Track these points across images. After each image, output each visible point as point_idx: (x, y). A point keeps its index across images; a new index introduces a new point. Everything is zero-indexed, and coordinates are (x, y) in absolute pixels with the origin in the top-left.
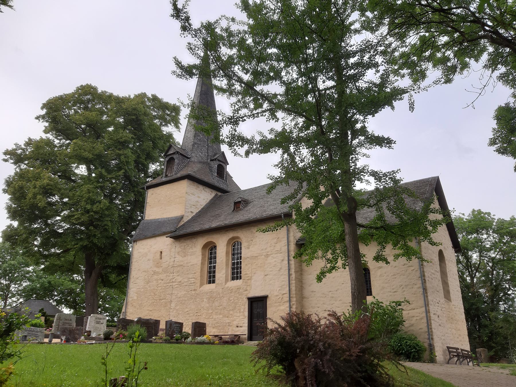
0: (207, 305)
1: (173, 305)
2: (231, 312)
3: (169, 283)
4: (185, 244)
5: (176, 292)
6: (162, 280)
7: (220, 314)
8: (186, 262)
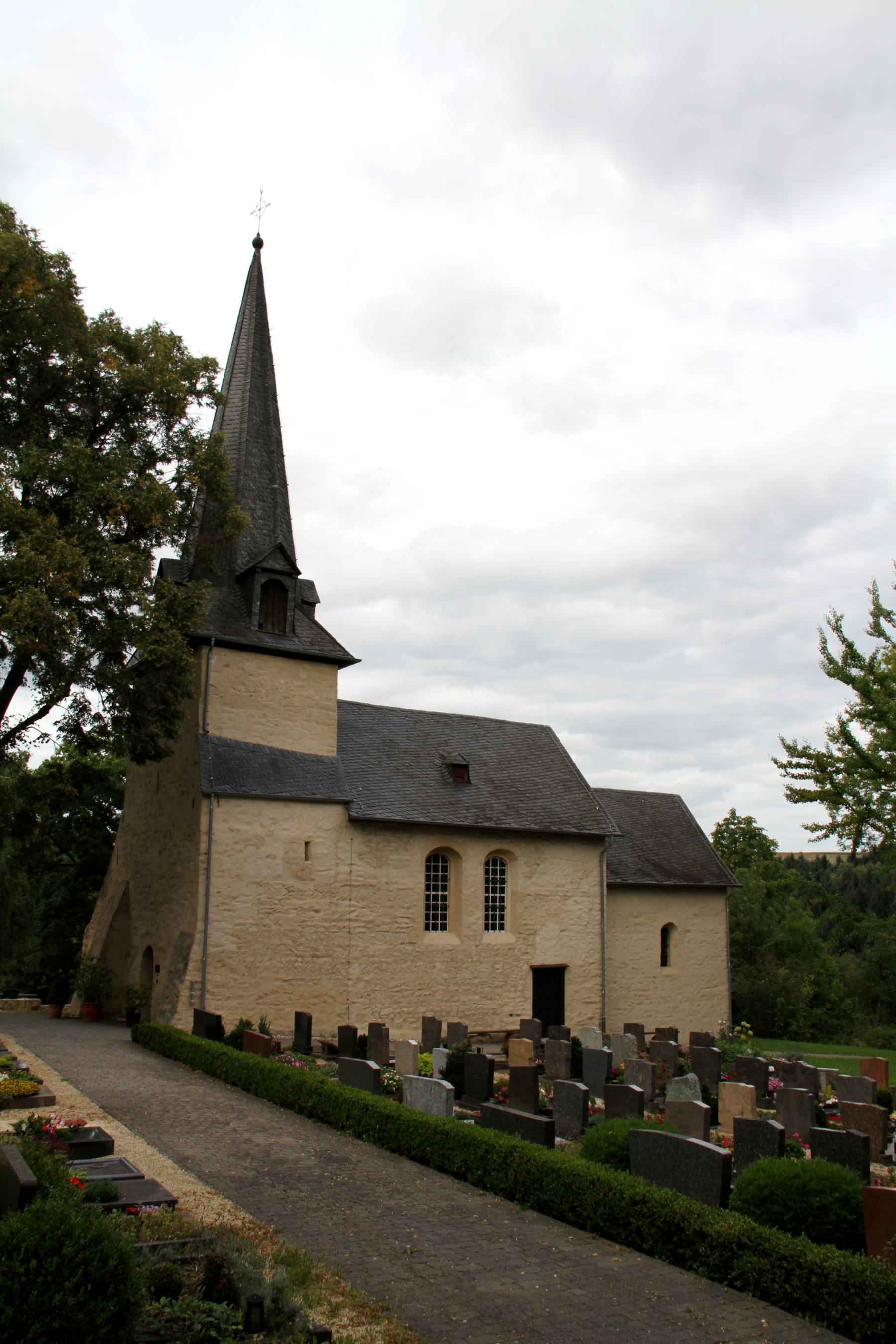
0: (445, 975)
1: (355, 970)
2: (499, 990)
3: (338, 921)
4: (379, 838)
5: (361, 943)
6: (317, 911)
7: (475, 993)
8: (385, 880)
